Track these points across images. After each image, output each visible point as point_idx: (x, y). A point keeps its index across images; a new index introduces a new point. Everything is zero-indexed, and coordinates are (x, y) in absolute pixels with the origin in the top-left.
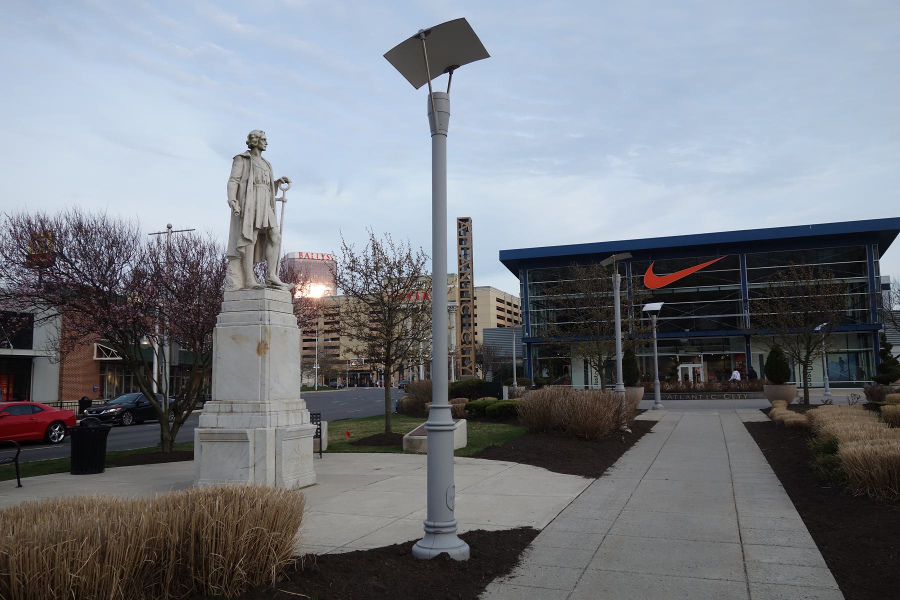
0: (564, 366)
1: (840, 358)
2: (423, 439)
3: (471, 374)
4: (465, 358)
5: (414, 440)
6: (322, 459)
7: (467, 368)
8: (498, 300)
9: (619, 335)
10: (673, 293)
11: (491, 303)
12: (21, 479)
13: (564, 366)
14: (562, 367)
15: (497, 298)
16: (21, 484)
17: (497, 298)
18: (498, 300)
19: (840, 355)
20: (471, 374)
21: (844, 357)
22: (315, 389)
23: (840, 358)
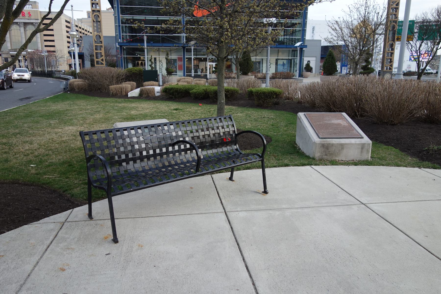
0: (136, 62)
1: (283, 62)
2: (346, 144)
3: (103, 64)
4: (97, 52)
5: (333, 145)
6: (267, 196)
7: (100, 60)
8: (66, 21)
9: (275, 28)
10: (145, 19)
11: (62, 23)
12: (267, 170)
13: (136, 62)
14: (135, 62)
15: (66, 20)
16: (268, 189)
17: (66, 20)
18: (66, 21)
19: (283, 61)
20: (103, 64)
21: (285, 62)
22: (205, 58)
23: (283, 62)
